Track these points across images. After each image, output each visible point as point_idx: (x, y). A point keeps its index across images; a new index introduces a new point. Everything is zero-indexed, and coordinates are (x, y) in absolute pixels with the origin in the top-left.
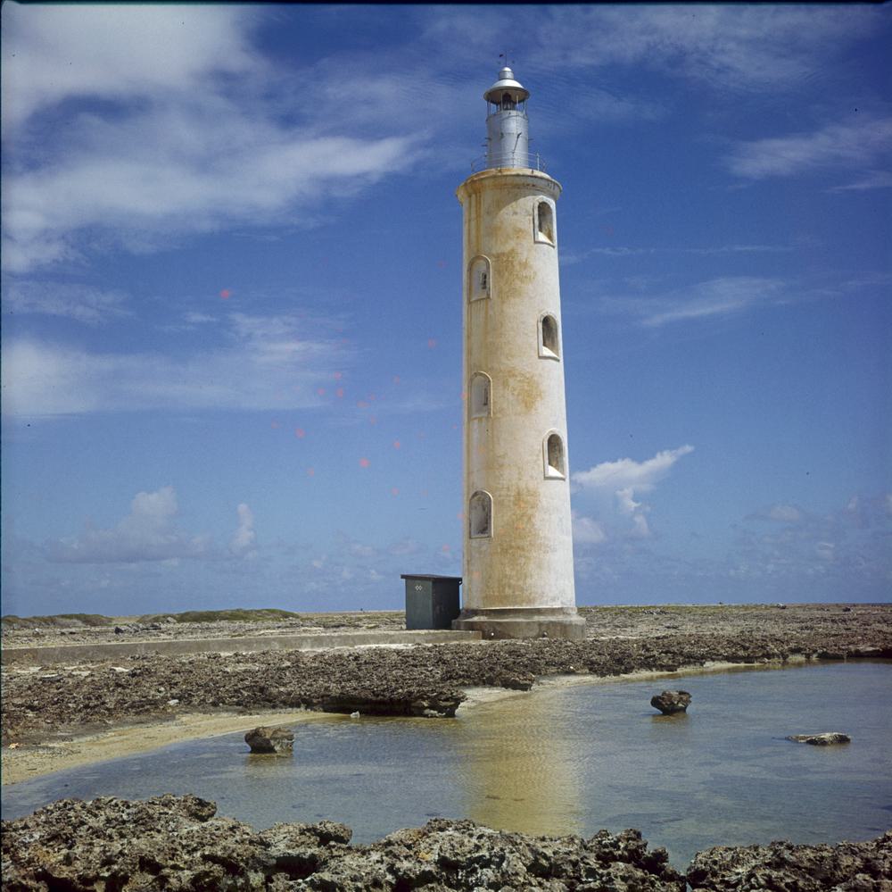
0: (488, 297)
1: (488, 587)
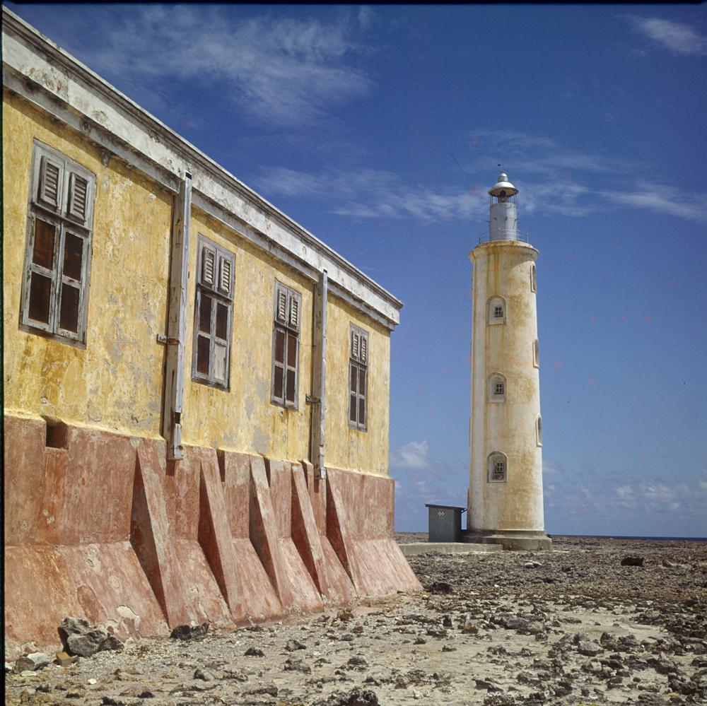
0: (505, 323)
1: (503, 515)
